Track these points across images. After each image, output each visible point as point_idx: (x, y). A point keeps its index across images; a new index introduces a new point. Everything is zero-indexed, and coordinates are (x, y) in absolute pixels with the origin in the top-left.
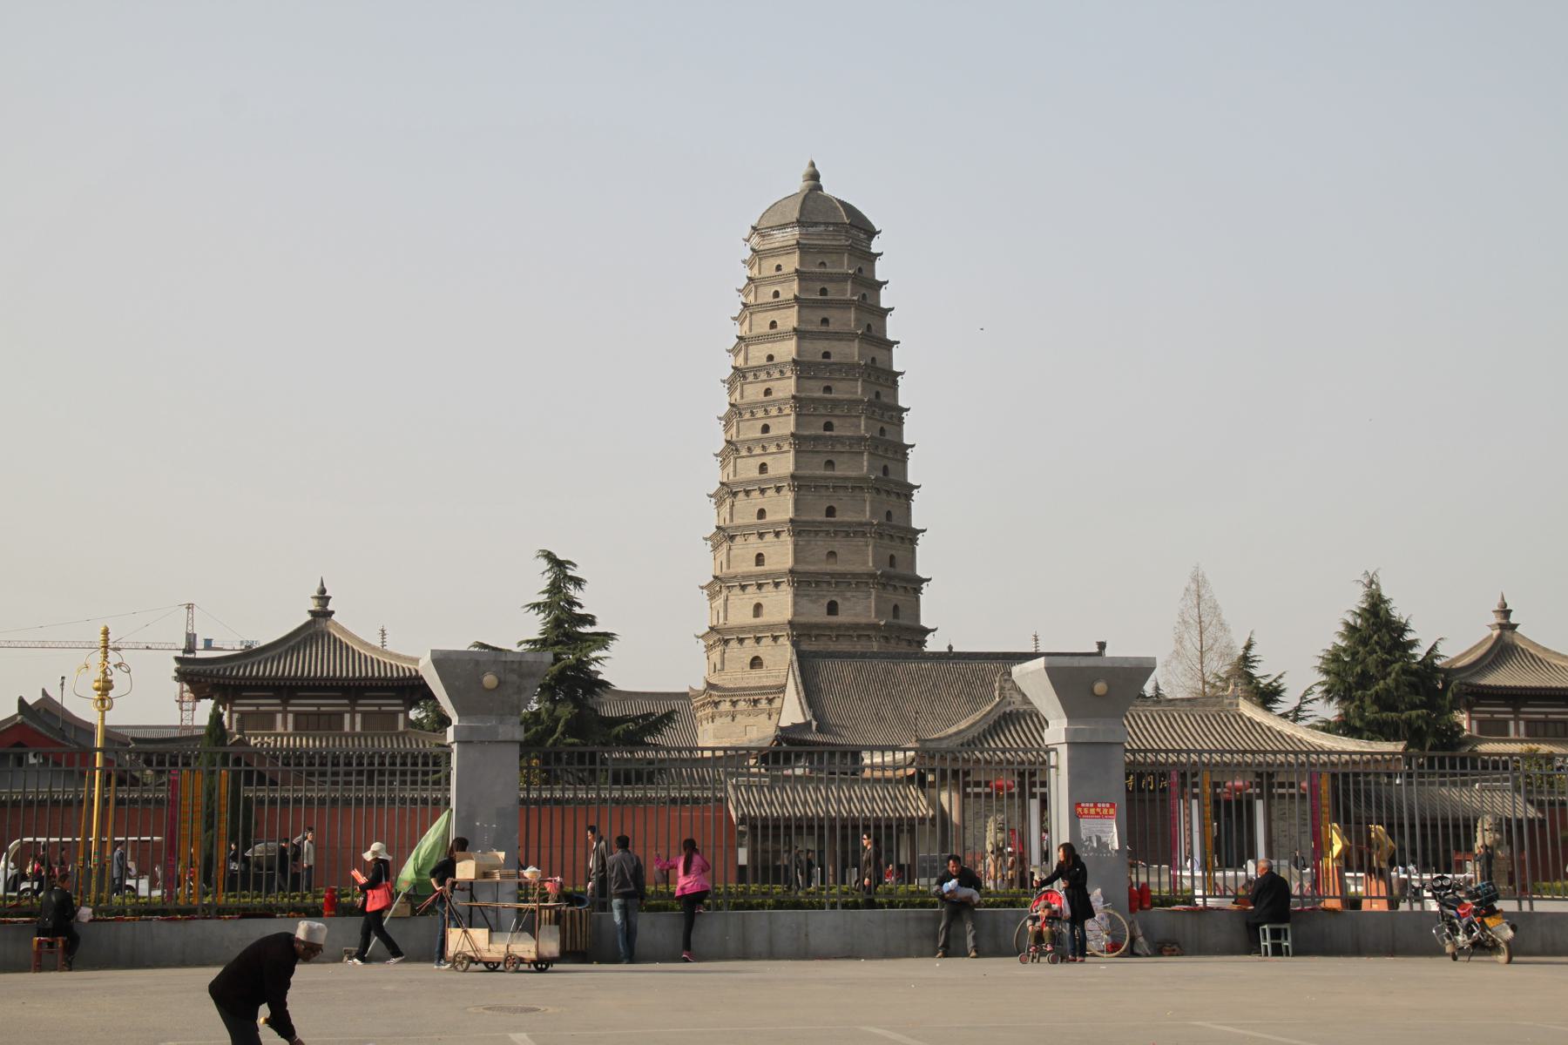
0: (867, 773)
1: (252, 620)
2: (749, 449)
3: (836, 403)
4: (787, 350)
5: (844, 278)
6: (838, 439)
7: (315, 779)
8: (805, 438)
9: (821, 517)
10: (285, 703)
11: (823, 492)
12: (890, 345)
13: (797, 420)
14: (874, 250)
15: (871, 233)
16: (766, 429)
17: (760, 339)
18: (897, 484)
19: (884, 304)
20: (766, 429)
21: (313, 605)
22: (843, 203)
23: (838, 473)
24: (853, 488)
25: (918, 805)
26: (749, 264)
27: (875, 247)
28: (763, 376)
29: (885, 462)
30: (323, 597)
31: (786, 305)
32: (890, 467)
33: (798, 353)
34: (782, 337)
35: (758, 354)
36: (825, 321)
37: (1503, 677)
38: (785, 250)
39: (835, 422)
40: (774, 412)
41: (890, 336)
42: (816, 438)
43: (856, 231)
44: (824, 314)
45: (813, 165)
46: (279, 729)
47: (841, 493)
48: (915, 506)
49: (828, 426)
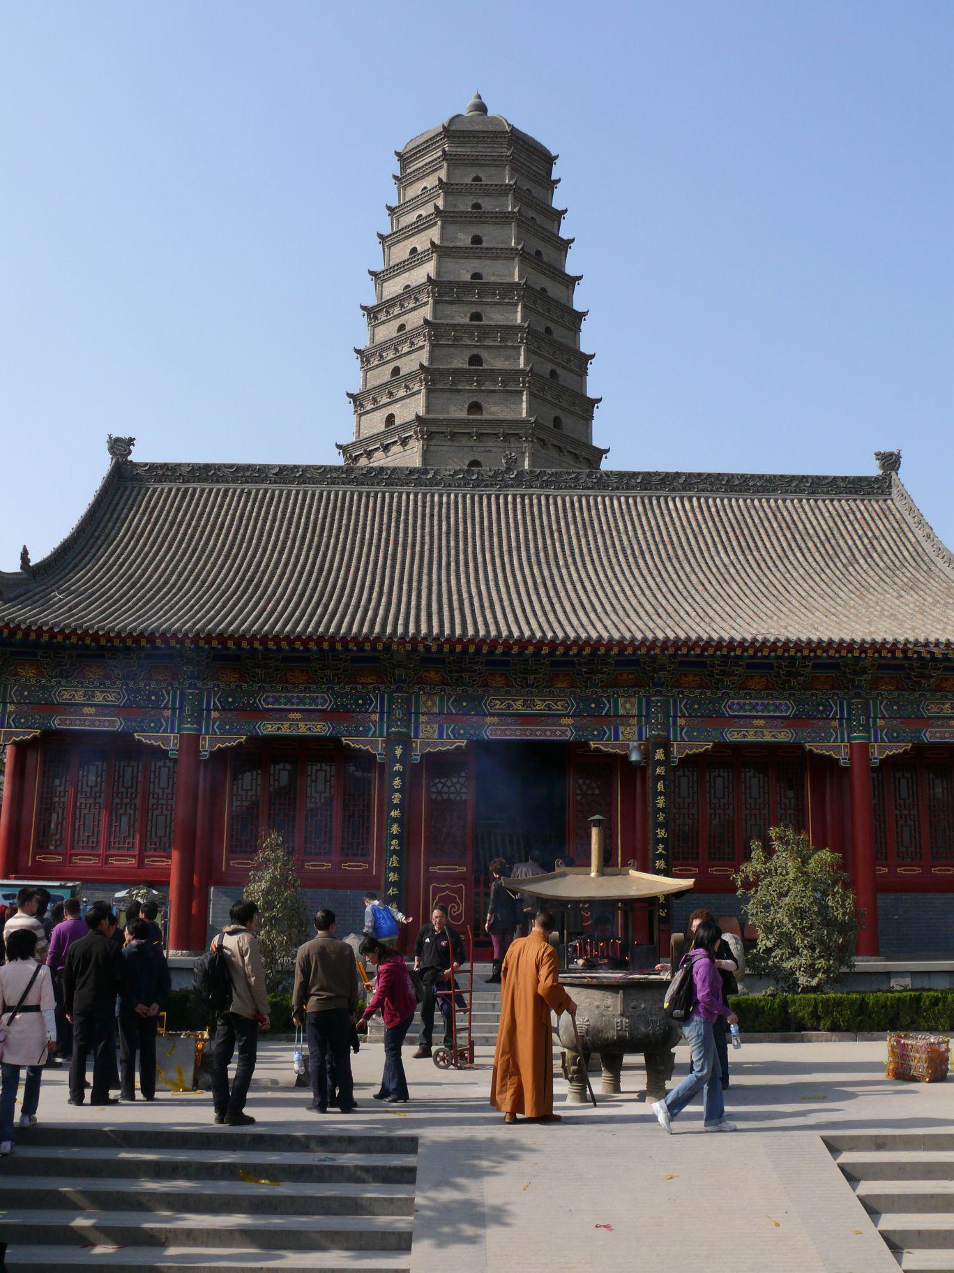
2: (375, 400)
3: (486, 332)
5: (502, 191)
6: (492, 374)
7: (818, 895)
8: (443, 373)
9: (467, 320)
11: (464, 441)
12: (564, 246)
13: (431, 352)
14: (554, 177)
18: (574, 442)
23: (485, 416)
24: (507, 436)
29: (558, 413)
32: (564, 419)
33: (438, 273)
39: (484, 354)
43: (533, 162)
44: (477, 230)
45: (479, 97)
47: (490, 443)
48: (596, 425)
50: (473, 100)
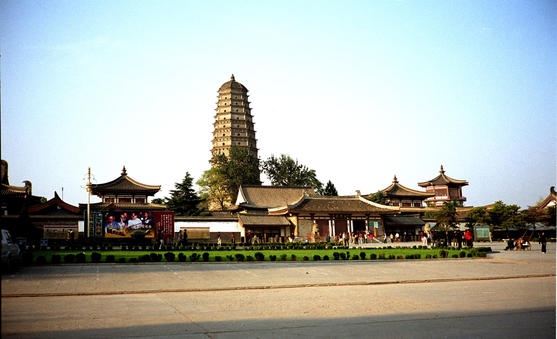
0: (270, 214)
1: (107, 175)
4: (229, 117)
6: (242, 138)
10: (116, 196)
15: (247, 91)
16: (224, 135)
17: (222, 114)
19: (250, 107)
20: (224, 135)
21: (122, 172)
22: (242, 85)
25: (285, 222)
26: (218, 97)
27: (248, 94)
28: (223, 123)
30: (124, 170)
31: (228, 106)
34: (228, 113)
35: (222, 117)
36: (237, 110)
37: (398, 193)
38: (227, 94)
40: (226, 131)
41: (252, 115)
42: (236, 137)
46: (132, 202)
49: (239, 135)
50: (231, 76)
